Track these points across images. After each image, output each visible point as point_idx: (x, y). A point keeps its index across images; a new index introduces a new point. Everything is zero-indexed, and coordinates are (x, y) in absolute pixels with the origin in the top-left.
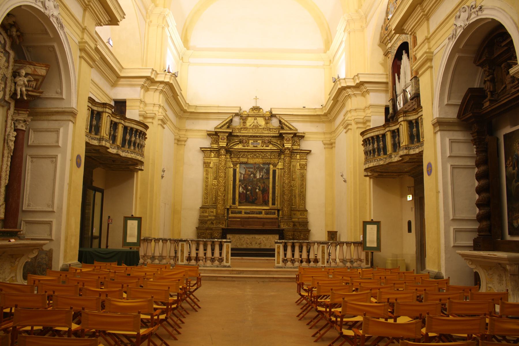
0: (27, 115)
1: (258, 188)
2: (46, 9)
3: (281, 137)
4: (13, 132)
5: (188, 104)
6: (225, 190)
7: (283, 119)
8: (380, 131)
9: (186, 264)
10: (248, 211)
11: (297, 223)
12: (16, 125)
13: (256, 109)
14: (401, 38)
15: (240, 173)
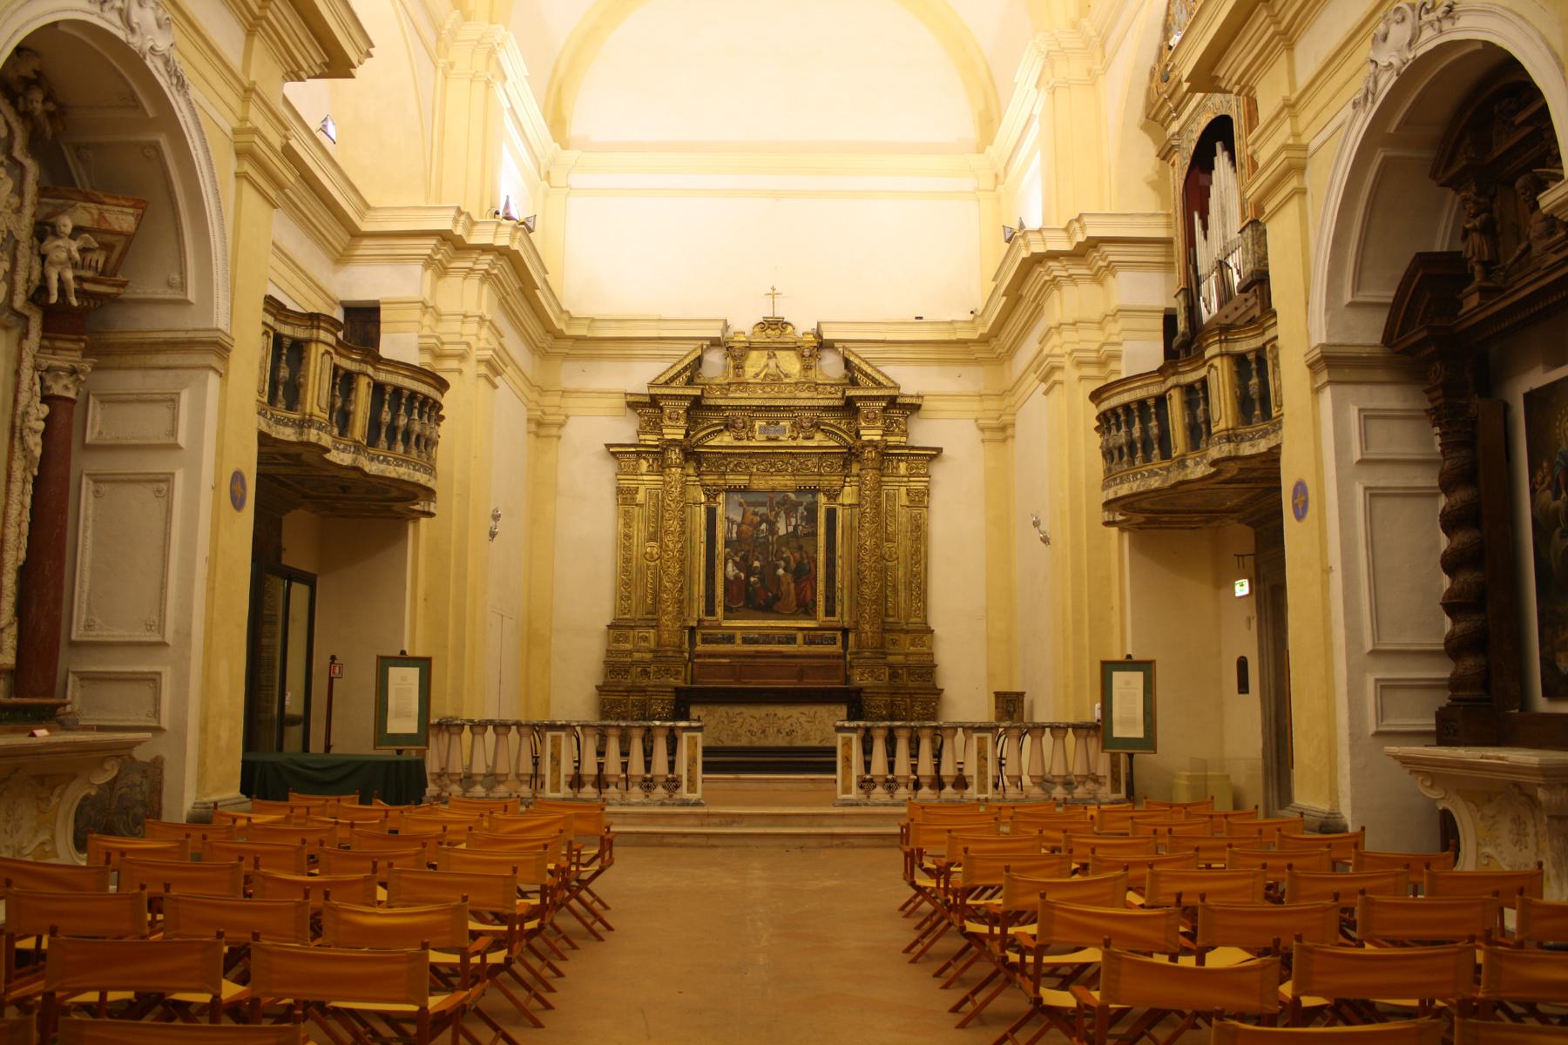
0: (79, 353)
1: (782, 563)
2: (132, 30)
3: (849, 408)
4: (39, 405)
5: (568, 312)
6: (681, 572)
7: (857, 356)
8: (1151, 388)
9: (567, 796)
10: (754, 634)
11: (902, 668)
12: (49, 383)
13: (775, 324)
14: (1209, 104)
15: (728, 518)
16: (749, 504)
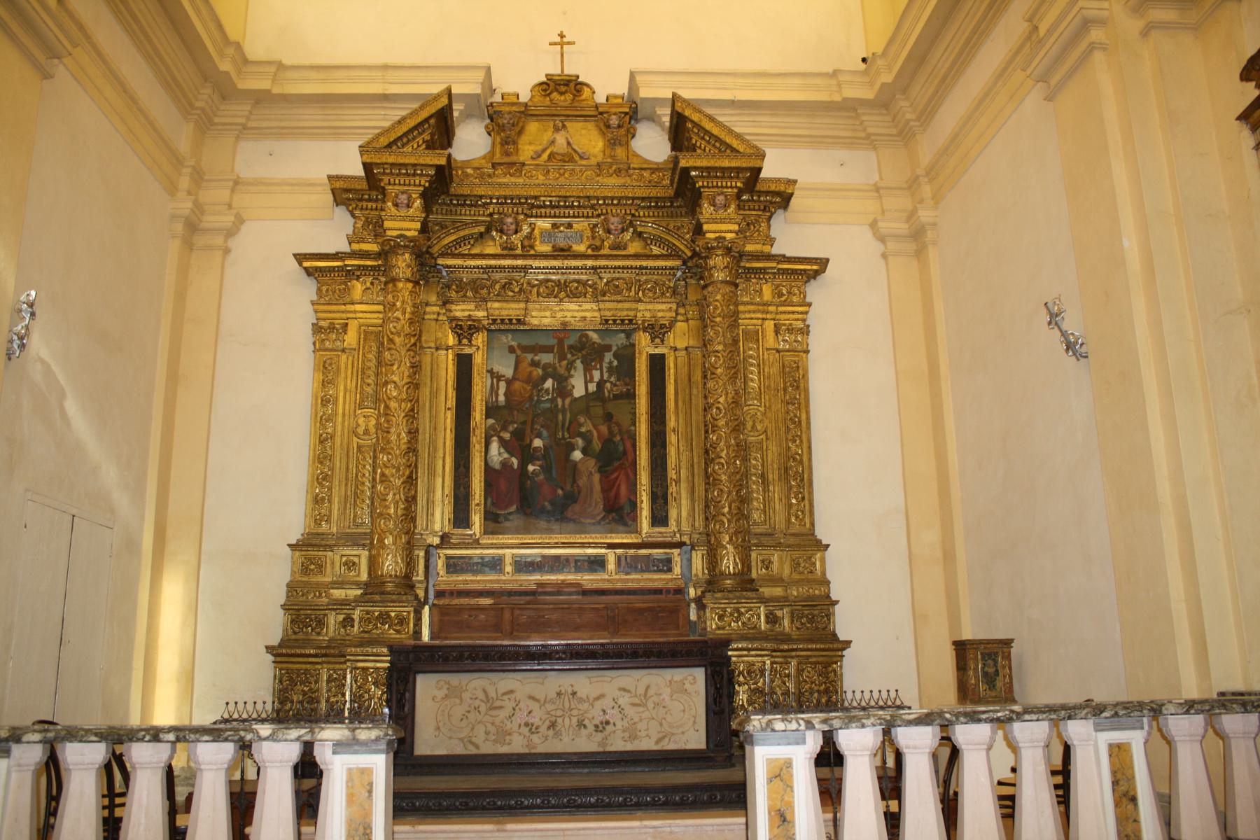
1: (580, 442)
15: (491, 372)
16: (526, 349)
